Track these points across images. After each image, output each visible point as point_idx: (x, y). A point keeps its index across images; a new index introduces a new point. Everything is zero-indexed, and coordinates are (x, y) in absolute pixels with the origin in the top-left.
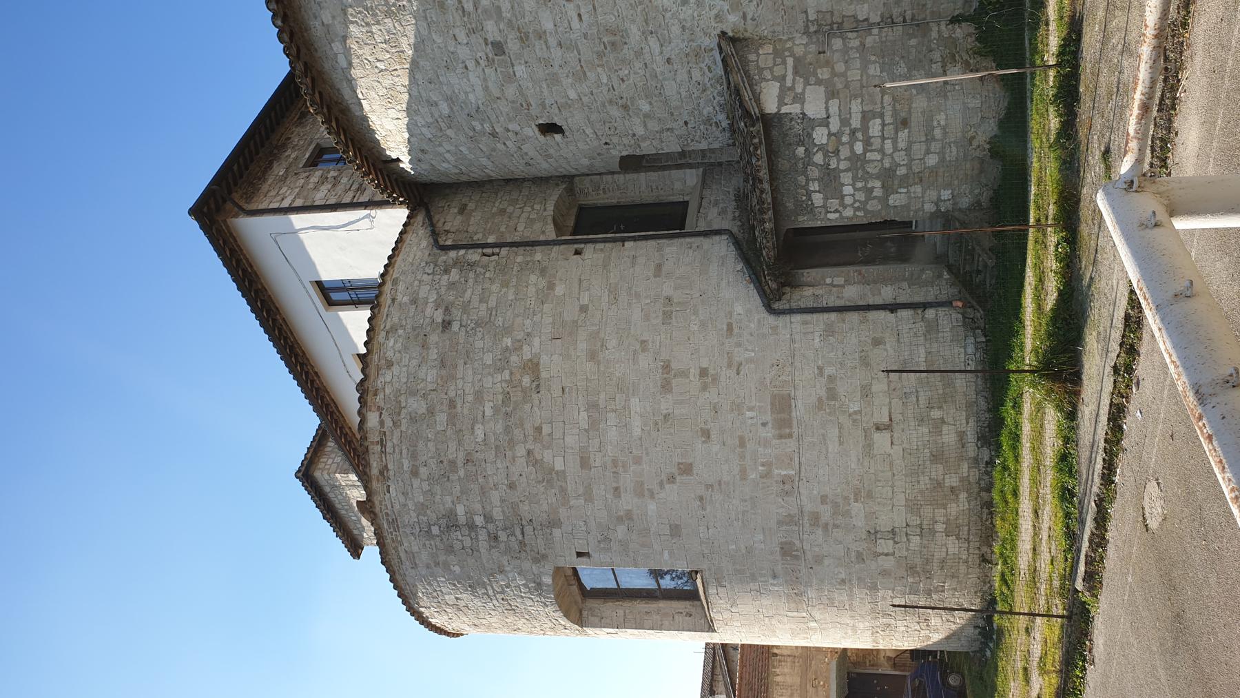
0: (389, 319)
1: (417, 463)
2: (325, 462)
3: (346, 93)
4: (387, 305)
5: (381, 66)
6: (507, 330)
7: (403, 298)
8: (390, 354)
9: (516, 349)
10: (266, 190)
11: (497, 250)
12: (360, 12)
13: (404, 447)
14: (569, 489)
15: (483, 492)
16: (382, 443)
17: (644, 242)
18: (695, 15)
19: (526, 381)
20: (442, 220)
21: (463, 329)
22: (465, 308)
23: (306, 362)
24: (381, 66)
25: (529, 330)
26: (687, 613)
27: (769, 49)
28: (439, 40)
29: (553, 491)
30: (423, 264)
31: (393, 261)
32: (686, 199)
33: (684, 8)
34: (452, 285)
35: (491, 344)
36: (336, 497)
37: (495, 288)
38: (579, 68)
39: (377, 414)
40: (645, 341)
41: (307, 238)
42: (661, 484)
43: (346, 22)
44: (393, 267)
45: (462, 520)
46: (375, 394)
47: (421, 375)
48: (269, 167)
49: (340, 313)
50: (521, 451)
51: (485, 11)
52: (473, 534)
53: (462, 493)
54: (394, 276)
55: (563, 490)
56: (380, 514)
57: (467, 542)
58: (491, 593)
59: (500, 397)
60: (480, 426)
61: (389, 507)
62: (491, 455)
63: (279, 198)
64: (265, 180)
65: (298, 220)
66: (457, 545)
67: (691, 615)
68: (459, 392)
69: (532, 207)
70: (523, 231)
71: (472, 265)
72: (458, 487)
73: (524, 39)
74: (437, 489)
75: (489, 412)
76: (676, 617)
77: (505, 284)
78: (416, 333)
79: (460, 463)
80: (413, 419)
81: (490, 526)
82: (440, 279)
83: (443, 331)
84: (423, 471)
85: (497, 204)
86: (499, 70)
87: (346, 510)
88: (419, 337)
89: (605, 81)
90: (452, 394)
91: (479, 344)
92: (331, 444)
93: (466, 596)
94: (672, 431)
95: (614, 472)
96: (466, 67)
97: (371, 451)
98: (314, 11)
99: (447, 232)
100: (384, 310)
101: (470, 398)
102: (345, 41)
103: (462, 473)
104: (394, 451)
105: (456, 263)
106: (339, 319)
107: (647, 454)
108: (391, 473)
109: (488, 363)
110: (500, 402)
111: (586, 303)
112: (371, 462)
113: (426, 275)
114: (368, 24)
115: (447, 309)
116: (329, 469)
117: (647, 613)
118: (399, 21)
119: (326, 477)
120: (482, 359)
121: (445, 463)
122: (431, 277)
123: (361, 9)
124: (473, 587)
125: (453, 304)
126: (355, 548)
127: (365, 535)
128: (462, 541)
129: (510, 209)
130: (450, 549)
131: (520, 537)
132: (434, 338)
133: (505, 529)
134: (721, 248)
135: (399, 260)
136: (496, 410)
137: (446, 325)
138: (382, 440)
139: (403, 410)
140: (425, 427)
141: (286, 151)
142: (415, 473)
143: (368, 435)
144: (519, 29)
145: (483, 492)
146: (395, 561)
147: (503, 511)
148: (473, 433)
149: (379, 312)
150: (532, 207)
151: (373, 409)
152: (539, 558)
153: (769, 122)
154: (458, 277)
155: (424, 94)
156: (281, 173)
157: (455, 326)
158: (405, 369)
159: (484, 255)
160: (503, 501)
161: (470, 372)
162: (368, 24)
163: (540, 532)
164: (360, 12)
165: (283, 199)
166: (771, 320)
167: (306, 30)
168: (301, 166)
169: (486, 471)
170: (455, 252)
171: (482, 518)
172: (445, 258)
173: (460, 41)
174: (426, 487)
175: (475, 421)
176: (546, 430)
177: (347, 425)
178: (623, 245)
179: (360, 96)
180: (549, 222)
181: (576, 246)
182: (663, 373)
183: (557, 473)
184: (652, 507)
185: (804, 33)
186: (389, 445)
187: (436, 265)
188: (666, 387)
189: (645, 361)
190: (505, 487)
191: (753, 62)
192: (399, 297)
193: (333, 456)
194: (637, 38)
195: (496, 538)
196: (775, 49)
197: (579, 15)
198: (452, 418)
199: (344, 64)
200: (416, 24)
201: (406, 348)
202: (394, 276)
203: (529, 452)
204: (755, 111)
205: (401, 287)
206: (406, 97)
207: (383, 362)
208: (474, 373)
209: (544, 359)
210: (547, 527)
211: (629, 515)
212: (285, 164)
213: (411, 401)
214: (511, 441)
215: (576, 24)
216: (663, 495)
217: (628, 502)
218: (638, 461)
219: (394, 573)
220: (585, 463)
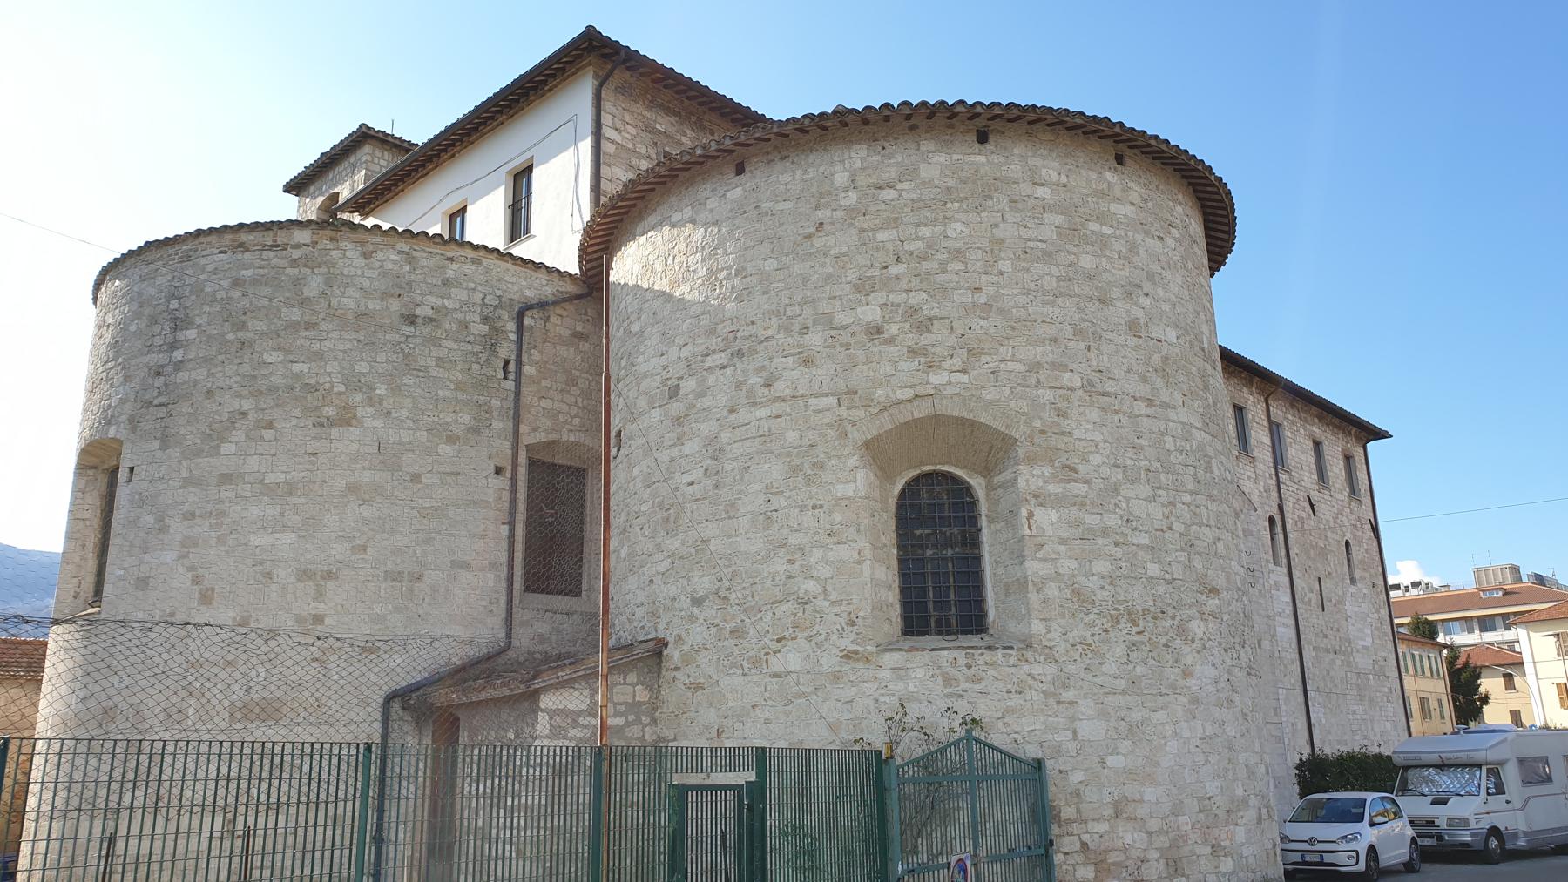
0: (425, 255)
1: (247, 286)
2: (382, 158)
3: (652, 219)
4: (443, 252)
5: (670, 261)
6: (396, 390)
7: (451, 271)
8: (380, 256)
9: (371, 399)
10: (634, 110)
11: (511, 376)
12: (713, 241)
13: (266, 271)
14: (200, 460)
15: (207, 360)
16: (274, 246)
17: (506, 548)
18: (683, 613)
19: (330, 411)
20: (565, 313)
21: (403, 339)
22: (433, 341)
23: (464, 144)
24: (670, 261)
25: (394, 415)
26: (78, 593)
27: (642, 694)
28: (685, 326)
29: (199, 442)
30: (499, 293)
31: (507, 258)
32: (584, 593)
33: (688, 600)
34: (465, 325)
35: (380, 371)
36: (345, 169)
37: (457, 375)
38: (654, 480)
39: (308, 241)
40: (365, 550)
41: (567, 158)
42: (192, 568)
43: (705, 224)
44: (497, 259)
45: (181, 336)
46: (332, 239)
47: (350, 291)
48: (669, 111)
49: (503, 188)
50: (247, 404)
51: (704, 380)
52: (165, 347)
53: (210, 337)
54: (484, 260)
55: (198, 453)
56: (197, 242)
57: (158, 341)
58: (110, 365)
59: (313, 382)
60: (281, 358)
61: (204, 253)
62: (246, 369)
63: (619, 125)
64: (650, 108)
65: (586, 146)
66: (157, 329)
67: (75, 597)
68: (325, 334)
69: (577, 416)
70: (539, 405)
71: (493, 348)
72: (216, 332)
73: (679, 421)
74: (217, 308)
75: (296, 368)
76: (75, 580)
77: (459, 387)
78: (404, 285)
79: (240, 335)
80: (298, 282)
81: (170, 368)
82: (474, 312)
83: (402, 316)
84: (237, 294)
85: (585, 375)
86: (658, 391)
87: (332, 180)
88: (397, 288)
89: (643, 509)
90: (323, 326)
91: (381, 357)
92: (401, 158)
93: (108, 337)
94: (252, 582)
95: (211, 513)
96: (662, 355)
97: (265, 233)
98: (719, 189)
99: (547, 319)
100: (438, 250)
101: (316, 346)
102: (690, 222)
103: (230, 336)
104: (263, 260)
105: (497, 331)
106: (498, 186)
107: (227, 552)
108: (239, 256)
109: (356, 367)
110: (307, 381)
111: (424, 480)
112: (255, 234)
113: (481, 296)
114: (703, 248)
115: (431, 320)
116: (372, 162)
117: (84, 546)
118: (703, 284)
119: (364, 159)
120: (362, 359)
121: (244, 318)
122: (480, 302)
123: (716, 242)
124: (114, 345)
125: (439, 327)
126: (297, 186)
127: (308, 200)
128: (160, 335)
129: (575, 391)
130: (153, 321)
131: (156, 402)
132: (395, 305)
133: (166, 385)
134: (489, 631)
135: (510, 266)
136: (297, 376)
137: (411, 320)
138: (278, 246)
139: (308, 271)
140: (287, 295)
141: (693, 130)
142: (237, 283)
143: (285, 230)
144: (686, 415)
145: (207, 360)
146: (149, 256)
147: (185, 383)
148: (274, 350)
149: (434, 243)
150: (577, 416)
151: (315, 236)
152: (133, 422)
153: (534, 695)
154: (476, 332)
155: (647, 305)
156: (658, 126)
157: (408, 330)
158: (359, 272)
159: (506, 364)
160: (196, 383)
161: (349, 346)
162: (703, 248)
163: (158, 426)
164: (713, 241)
165: (617, 130)
166: (378, 698)
167: (703, 179)
168: (667, 149)
169: (229, 364)
170: (514, 330)
171: (180, 359)
172: (506, 317)
173: (683, 349)
174: (221, 294)
175: (288, 352)
176: (268, 434)
177: (406, 187)
178: (504, 523)
179: (650, 234)
180: (550, 436)
181: (509, 468)
182: (322, 571)
183: (218, 446)
184: (169, 556)
185: (659, 737)
186: (271, 254)
187: (496, 307)
188: (305, 575)
189: (339, 550)
190: (209, 385)
191: (625, 679)
192: (454, 266)
193: (384, 162)
194: (671, 547)
195: (158, 374)
196: (641, 704)
197: (692, 483)
198: (293, 326)
199: (676, 217)
200: (699, 302)
201: (385, 274)
202: (484, 260)
203: (244, 414)
204: (539, 683)
205: (468, 268)
206: (645, 286)
207: (371, 248)
208: (344, 351)
209: (355, 432)
210: (162, 434)
211: (164, 529)
212: (671, 130)
213: (320, 280)
214: (261, 393)
215: (687, 478)
216: (181, 570)
217: (178, 528)
218: (221, 541)
219: (139, 255)
220: (226, 479)
